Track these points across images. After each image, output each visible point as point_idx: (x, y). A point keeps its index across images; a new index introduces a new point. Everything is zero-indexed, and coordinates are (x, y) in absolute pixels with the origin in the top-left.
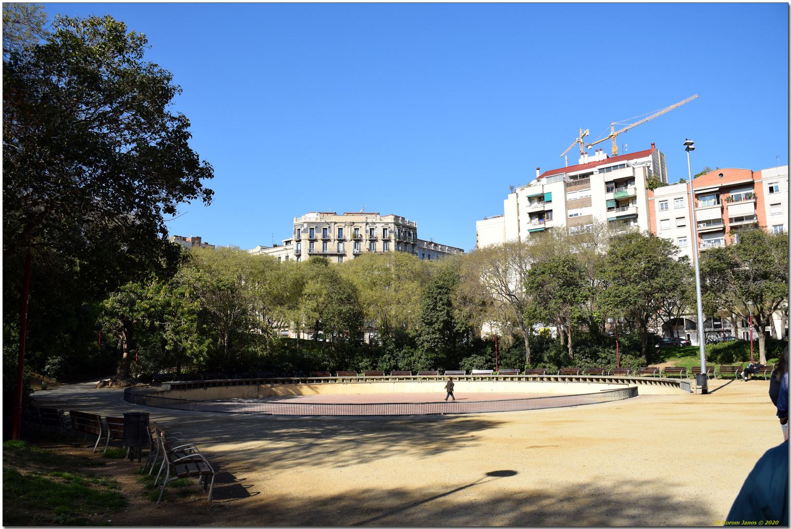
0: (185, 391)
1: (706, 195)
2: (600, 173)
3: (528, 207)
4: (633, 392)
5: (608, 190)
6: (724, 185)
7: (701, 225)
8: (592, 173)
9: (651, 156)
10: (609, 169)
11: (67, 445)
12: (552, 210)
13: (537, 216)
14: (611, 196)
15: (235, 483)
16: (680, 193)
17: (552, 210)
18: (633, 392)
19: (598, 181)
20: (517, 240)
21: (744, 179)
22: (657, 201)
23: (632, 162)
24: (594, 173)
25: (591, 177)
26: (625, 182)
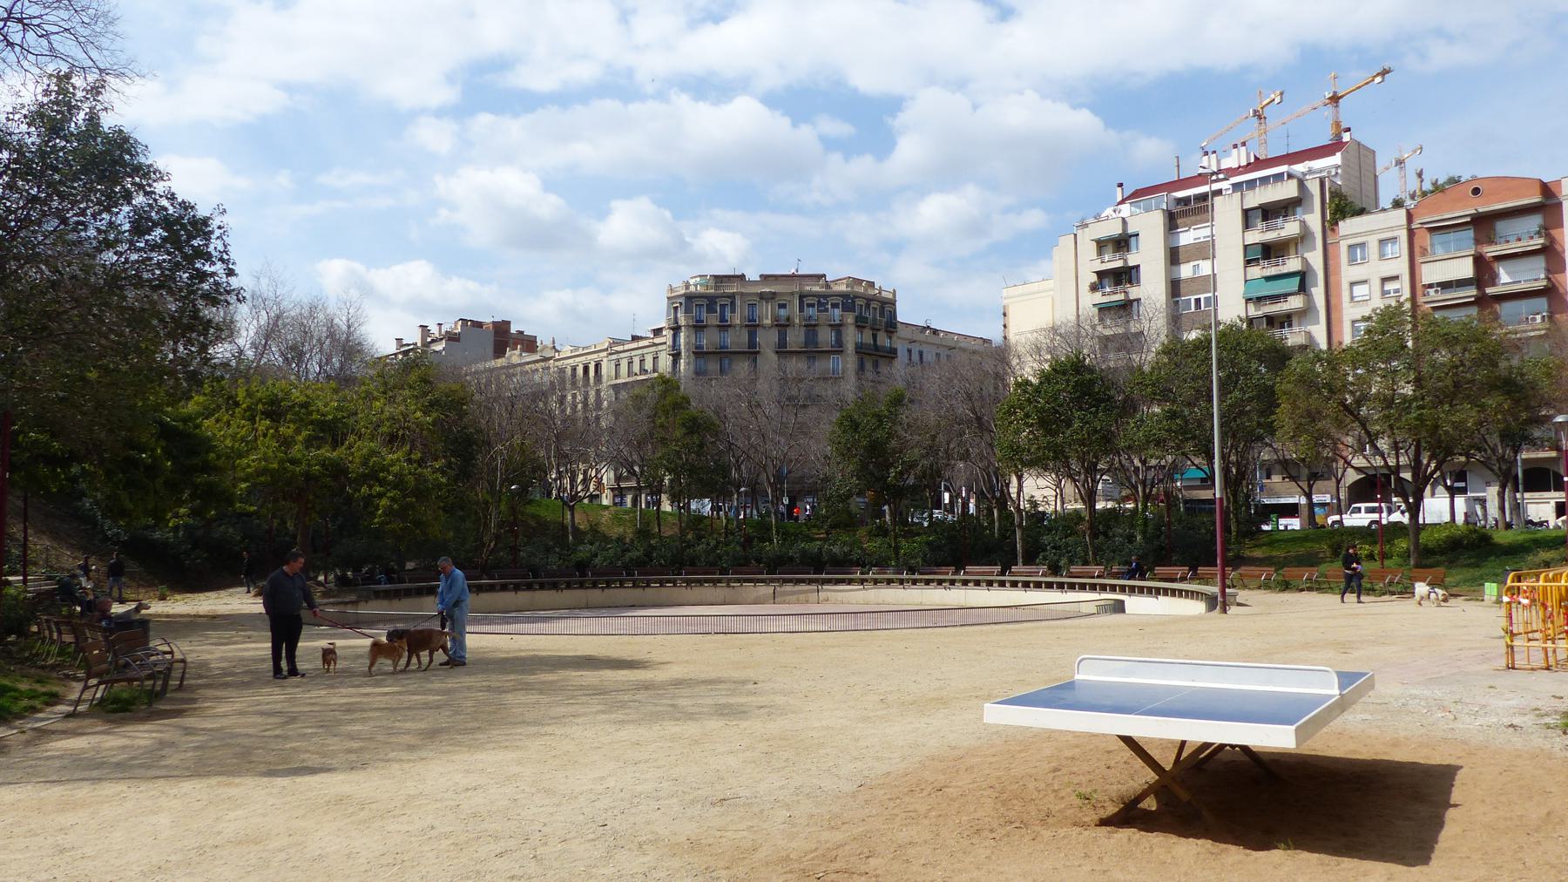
0: (400, 600)
1: (1452, 230)
2: (1233, 192)
3: (1092, 263)
4: (1119, 607)
5: (1247, 225)
6: (1480, 210)
7: (1431, 291)
8: (1219, 192)
9: (1339, 155)
10: (1251, 184)
11: (1421, 509)
12: (1139, 266)
13: (1112, 277)
14: (1098, 298)
15: (1213, 747)
16: (1391, 229)
17: (1139, 266)
18: (1119, 607)
19: (1227, 211)
20: (1073, 318)
21: (1524, 196)
22: (1344, 245)
23: (1299, 168)
24: (1224, 193)
25: (1217, 199)
26: (1283, 208)
